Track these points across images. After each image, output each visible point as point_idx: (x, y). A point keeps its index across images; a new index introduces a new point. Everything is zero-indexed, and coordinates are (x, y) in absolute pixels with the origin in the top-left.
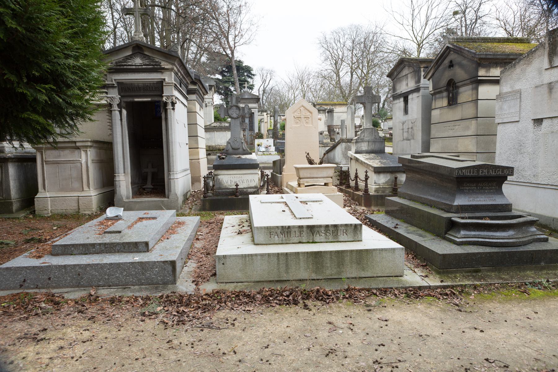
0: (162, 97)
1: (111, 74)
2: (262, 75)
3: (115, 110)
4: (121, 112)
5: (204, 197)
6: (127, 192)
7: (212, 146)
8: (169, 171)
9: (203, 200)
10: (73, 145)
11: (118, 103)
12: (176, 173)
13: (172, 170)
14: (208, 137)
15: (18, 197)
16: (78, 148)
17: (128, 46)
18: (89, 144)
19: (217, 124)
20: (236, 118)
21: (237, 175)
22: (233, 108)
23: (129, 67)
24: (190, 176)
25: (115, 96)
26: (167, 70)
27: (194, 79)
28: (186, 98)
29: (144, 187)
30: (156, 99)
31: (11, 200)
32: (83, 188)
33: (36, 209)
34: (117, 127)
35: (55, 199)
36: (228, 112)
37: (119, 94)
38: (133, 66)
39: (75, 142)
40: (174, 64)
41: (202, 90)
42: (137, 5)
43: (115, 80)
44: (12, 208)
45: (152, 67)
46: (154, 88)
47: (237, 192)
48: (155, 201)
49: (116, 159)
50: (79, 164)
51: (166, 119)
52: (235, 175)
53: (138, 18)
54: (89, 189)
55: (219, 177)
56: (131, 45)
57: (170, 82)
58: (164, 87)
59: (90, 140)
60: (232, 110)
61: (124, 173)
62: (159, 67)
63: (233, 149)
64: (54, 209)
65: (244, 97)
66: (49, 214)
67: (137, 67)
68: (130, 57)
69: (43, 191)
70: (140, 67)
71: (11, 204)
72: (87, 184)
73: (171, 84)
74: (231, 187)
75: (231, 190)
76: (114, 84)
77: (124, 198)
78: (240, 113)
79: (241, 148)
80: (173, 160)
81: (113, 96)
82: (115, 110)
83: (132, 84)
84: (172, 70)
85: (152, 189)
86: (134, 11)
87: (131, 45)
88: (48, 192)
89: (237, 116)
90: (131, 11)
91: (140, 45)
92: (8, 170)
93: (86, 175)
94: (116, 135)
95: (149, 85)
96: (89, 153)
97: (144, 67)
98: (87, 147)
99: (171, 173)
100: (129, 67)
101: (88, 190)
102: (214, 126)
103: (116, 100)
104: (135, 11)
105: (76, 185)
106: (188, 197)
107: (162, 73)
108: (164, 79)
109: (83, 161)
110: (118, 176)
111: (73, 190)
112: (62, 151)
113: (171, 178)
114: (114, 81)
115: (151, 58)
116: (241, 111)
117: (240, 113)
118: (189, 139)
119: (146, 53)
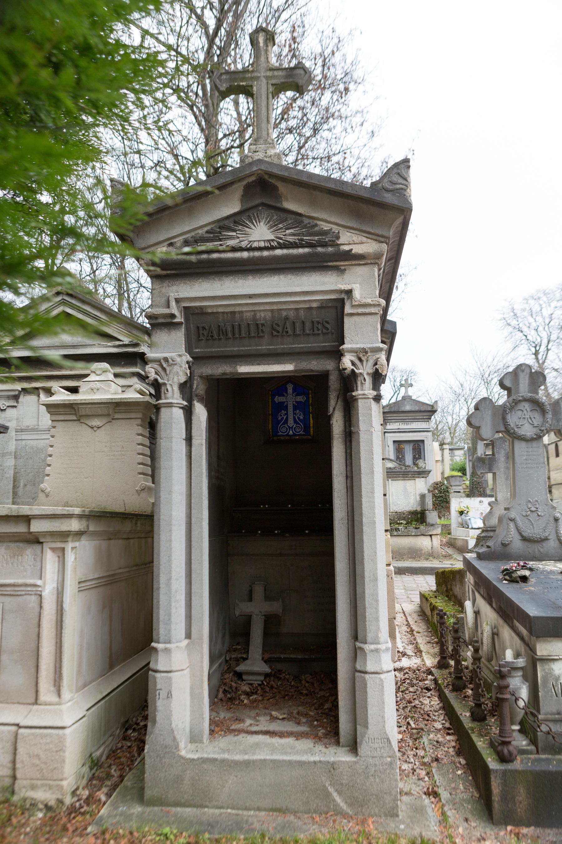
1: (166, 283)
2: (392, 380)
3: (170, 405)
4: (188, 412)
6: (192, 712)
10: (21, 529)
11: (183, 379)
13: (370, 636)
17: (232, 183)
18: (75, 525)
20: (532, 440)
25: (173, 355)
26: (360, 258)
29: (241, 668)
30: (328, 365)
32: (37, 692)
34: (175, 463)
36: (504, 419)
37: (189, 350)
38: (241, 249)
39: (27, 519)
42: (263, 59)
43: (178, 301)
45: (306, 250)
46: (308, 326)
48: (301, 764)
49: (162, 585)
50: (33, 599)
54: (59, 695)
56: (240, 180)
58: (346, 320)
59: (77, 511)
61: (188, 635)
62: (330, 249)
63: (525, 539)
65: (403, 409)
67: (257, 254)
70: (266, 253)
72: (52, 676)
73: (373, 310)
76: (173, 316)
78: (545, 421)
79: (552, 537)
82: (170, 405)
83: (233, 313)
85: (267, 675)
86: (252, 78)
87: (240, 180)
89: (536, 430)
90: (243, 79)
91: (271, 175)
93: (53, 641)
94: (170, 493)
95: (292, 314)
96: (70, 557)
97: (278, 252)
98: (64, 536)
101: (54, 699)
103: (176, 368)
104: (257, 78)
108: (349, 292)
113: (369, 668)
114: (173, 304)
115: (306, 221)
116: (549, 416)
117: (545, 421)
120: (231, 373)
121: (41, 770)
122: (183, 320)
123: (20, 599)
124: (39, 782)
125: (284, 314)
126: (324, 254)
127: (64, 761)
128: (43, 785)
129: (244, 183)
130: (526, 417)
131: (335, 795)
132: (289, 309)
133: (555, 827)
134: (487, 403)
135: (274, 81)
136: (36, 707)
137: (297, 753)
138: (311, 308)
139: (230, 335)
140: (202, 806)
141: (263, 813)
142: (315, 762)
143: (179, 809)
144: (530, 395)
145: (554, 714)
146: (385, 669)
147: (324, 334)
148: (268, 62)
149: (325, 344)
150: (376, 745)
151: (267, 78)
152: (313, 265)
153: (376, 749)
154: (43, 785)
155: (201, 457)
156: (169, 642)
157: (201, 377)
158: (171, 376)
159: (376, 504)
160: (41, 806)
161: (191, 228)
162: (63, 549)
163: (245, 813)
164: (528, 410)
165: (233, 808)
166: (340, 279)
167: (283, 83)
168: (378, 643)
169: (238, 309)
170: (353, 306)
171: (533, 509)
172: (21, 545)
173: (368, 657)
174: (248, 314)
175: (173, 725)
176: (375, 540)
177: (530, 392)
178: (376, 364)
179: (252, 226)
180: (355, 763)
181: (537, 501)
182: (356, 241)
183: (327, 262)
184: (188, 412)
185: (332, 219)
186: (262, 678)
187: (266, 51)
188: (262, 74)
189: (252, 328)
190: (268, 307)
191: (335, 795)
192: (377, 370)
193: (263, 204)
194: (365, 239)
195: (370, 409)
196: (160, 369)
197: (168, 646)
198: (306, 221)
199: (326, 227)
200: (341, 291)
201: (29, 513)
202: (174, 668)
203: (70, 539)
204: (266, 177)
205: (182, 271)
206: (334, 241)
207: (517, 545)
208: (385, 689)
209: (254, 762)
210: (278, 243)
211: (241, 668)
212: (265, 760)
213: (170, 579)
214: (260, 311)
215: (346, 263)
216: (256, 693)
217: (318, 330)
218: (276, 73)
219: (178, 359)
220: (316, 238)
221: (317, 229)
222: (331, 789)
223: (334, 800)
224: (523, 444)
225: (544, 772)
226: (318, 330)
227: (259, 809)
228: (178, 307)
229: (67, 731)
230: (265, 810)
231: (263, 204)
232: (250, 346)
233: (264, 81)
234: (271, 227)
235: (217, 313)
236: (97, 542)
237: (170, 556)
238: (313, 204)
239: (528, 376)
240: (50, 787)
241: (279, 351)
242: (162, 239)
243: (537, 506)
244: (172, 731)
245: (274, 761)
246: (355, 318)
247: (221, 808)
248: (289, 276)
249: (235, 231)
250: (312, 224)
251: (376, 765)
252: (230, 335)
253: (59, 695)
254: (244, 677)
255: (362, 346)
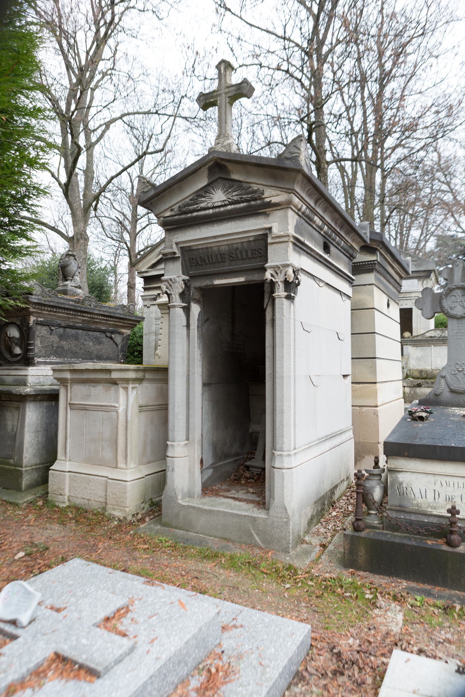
0: (264, 270)
3: (174, 306)
4: (187, 310)
5: (356, 529)
7: (426, 372)
8: (274, 448)
9: (352, 537)
11: (181, 291)
12: (289, 455)
14: (419, 356)
15: (38, 462)
16: (114, 382)
17: (200, 168)
19: (438, 333)
21: (456, 480)
22: (454, 293)
23: (202, 213)
24: (352, 441)
25: (174, 276)
27: (368, 241)
28: (350, 281)
30: (255, 277)
31: (22, 467)
33: (50, 490)
35: (75, 476)
36: (440, 303)
38: (208, 208)
40: (292, 191)
41: (393, 268)
42: (223, 81)
43: (177, 244)
44: (21, 483)
45: (245, 204)
47: (452, 532)
48: (238, 516)
51: (273, 321)
52: (448, 479)
53: (224, 107)
55: (401, 477)
56: (205, 165)
57: (282, 233)
58: (269, 247)
60: (453, 298)
63: (452, 391)
64: (72, 495)
66: (64, 503)
67: (217, 210)
68: (205, 191)
69: (63, 458)
70: (222, 209)
71: (20, 474)
73: (285, 239)
74: (435, 512)
75: (435, 520)
76: (175, 253)
77: (179, 497)
80: (282, 422)
81: (171, 277)
82: (174, 306)
84: (287, 205)
87: (205, 165)
88: (70, 460)
90: (212, 97)
91: (222, 159)
92: (24, 416)
95: (239, 246)
97: (229, 207)
98: (127, 381)
99: (277, 453)
100: (202, 213)
102: (431, 337)
103: (177, 284)
105: (108, 454)
106: (335, 497)
107: (266, 215)
108: (270, 229)
109: (121, 409)
110: (172, 446)
111: (102, 463)
112: (93, 387)
114: (174, 246)
115: (245, 185)
118: (352, 363)
119: (235, 176)
120: (211, 285)
121: (117, 501)
122: (180, 255)
123: (109, 413)
124: (116, 507)
125: (235, 246)
126: (255, 206)
127: (126, 498)
128: (118, 509)
129: (207, 166)
130: (458, 300)
131: (255, 535)
132: (238, 243)
133: (382, 575)
134: (428, 291)
135: (229, 95)
136: (116, 469)
137: (243, 510)
138: (249, 241)
139: (207, 262)
140: (188, 531)
141: (217, 539)
142: (245, 516)
143: (177, 530)
144: (462, 284)
145: (397, 506)
146: (286, 467)
147: (260, 257)
148: (226, 82)
149: (256, 264)
150: (279, 511)
151: (226, 93)
152: (250, 213)
153: (278, 513)
154: (118, 509)
155: (194, 336)
156: (174, 441)
157: (195, 288)
158: (174, 289)
159: (285, 365)
160: (117, 519)
161: (182, 198)
162: (127, 388)
163: (208, 537)
164: (460, 295)
165: (203, 534)
166: (266, 220)
167: (235, 95)
168: (283, 451)
169: (209, 246)
170: (273, 238)
171: (460, 369)
172: (109, 385)
173: (276, 459)
174: (215, 248)
175: (175, 486)
176: (283, 388)
177: (462, 282)
178: (286, 275)
179: (214, 193)
180: (267, 519)
181: (463, 363)
182: (274, 194)
183: (258, 210)
184: (187, 310)
185: (259, 182)
186: (261, 470)
187: (225, 75)
188: (223, 91)
189: (219, 257)
190: (225, 243)
191: (255, 535)
192: (286, 279)
193: (220, 178)
194: (280, 192)
195: (283, 304)
196: (168, 286)
197: (173, 443)
198: (245, 185)
199: (255, 187)
200: (266, 229)
201: (110, 368)
202: (175, 456)
203: (130, 382)
204: (219, 161)
205: (180, 225)
206: (260, 196)
207: (446, 395)
208: (285, 479)
209: (214, 511)
210: (229, 202)
211: (248, 463)
212: (219, 511)
213: (174, 407)
214: (222, 245)
215: (270, 209)
216: (253, 478)
217: (256, 254)
218: (231, 89)
219: (178, 279)
220: (250, 196)
221: (250, 189)
222: (253, 532)
223: (255, 538)
224: (455, 322)
225: (378, 540)
226: (256, 254)
227: (216, 537)
228: (177, 248)
229: (128, 483)
230: (219, 538)
231: (220, 178)
232: (219, 267)
233: (224, 95)
234: (225, 192)
235: (199, 249)
236: (159, 385)
237: (174, 394)
238: (248, 173)
239: (461, 269)
240: (121, 510)
241: (236, 270)
242: (167, 207)
243: (464, 367)
244: (174, 489)
245: (224, 512)
246: (275, 245)
247: (197, 533)
248: (237, 222)
249: (205, 197)
250: (248, 186)
251: (278, 522)
252: (207, 262)
253: (127, 465)
254: (250, 469)
255: (275, 264)
